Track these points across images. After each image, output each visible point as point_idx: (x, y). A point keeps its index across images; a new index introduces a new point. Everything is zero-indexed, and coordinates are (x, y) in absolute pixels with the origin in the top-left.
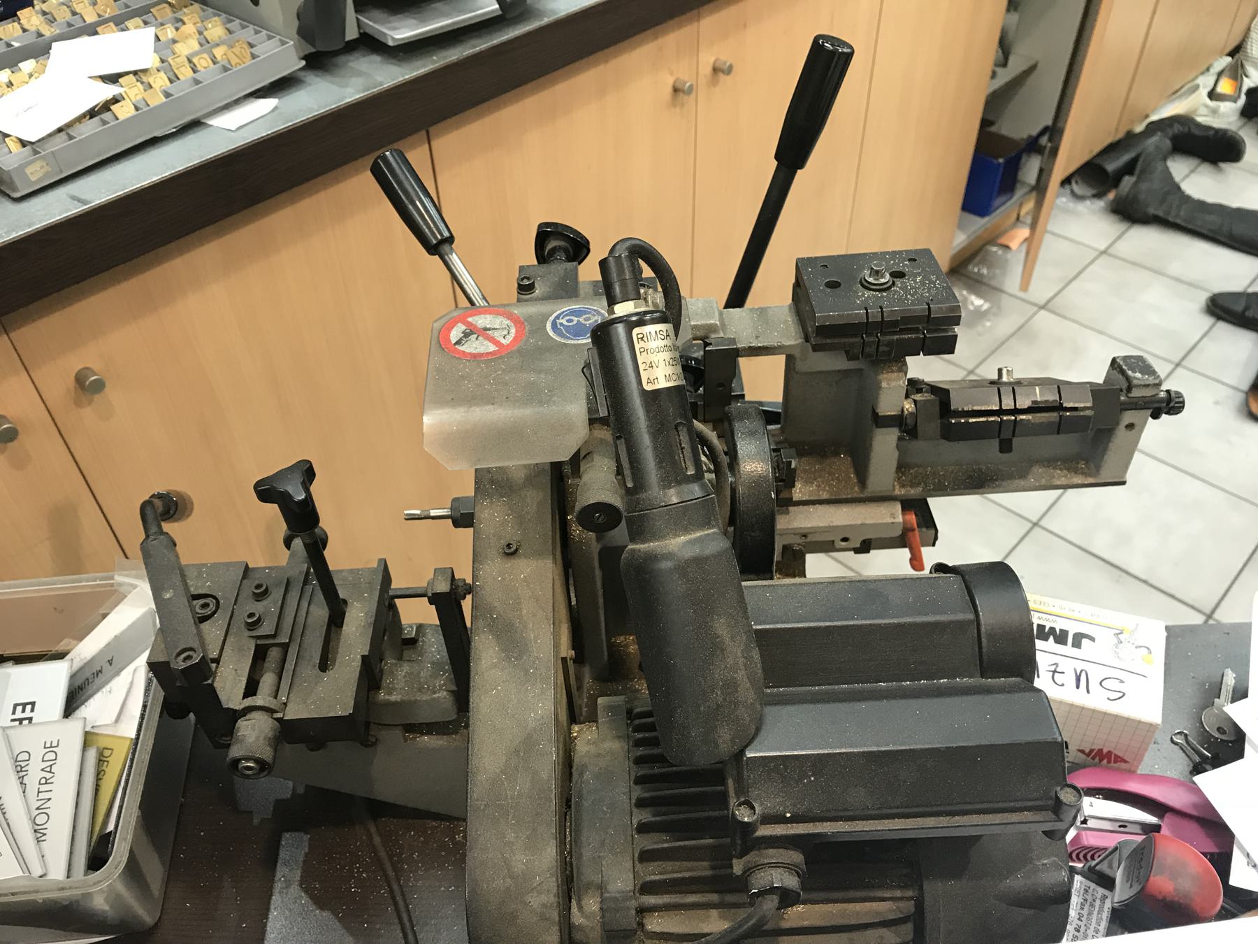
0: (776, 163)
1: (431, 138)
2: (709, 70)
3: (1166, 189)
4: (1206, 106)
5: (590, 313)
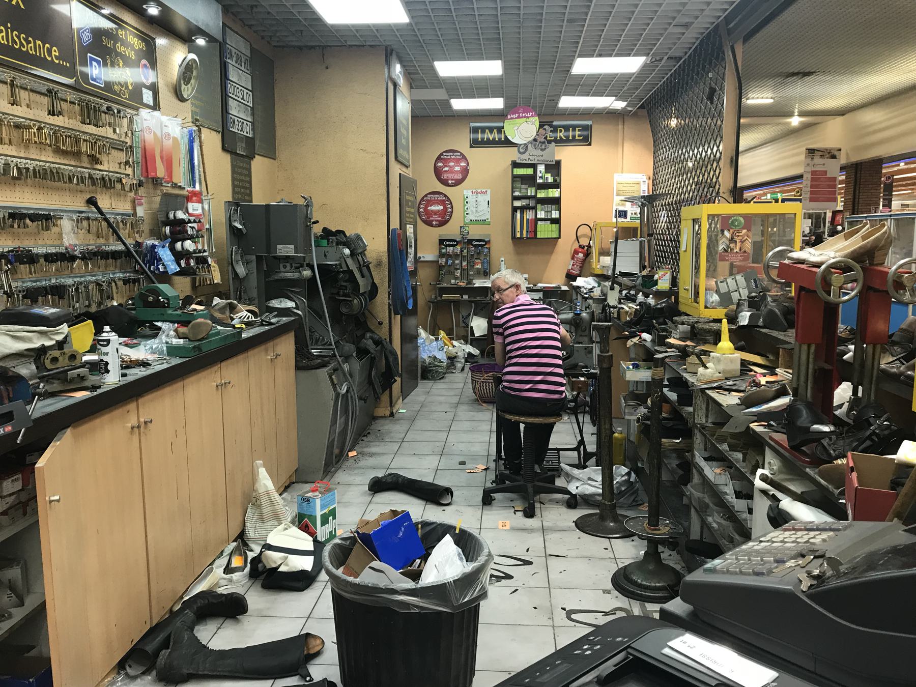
4: (225, 579)
5: (881, 220)
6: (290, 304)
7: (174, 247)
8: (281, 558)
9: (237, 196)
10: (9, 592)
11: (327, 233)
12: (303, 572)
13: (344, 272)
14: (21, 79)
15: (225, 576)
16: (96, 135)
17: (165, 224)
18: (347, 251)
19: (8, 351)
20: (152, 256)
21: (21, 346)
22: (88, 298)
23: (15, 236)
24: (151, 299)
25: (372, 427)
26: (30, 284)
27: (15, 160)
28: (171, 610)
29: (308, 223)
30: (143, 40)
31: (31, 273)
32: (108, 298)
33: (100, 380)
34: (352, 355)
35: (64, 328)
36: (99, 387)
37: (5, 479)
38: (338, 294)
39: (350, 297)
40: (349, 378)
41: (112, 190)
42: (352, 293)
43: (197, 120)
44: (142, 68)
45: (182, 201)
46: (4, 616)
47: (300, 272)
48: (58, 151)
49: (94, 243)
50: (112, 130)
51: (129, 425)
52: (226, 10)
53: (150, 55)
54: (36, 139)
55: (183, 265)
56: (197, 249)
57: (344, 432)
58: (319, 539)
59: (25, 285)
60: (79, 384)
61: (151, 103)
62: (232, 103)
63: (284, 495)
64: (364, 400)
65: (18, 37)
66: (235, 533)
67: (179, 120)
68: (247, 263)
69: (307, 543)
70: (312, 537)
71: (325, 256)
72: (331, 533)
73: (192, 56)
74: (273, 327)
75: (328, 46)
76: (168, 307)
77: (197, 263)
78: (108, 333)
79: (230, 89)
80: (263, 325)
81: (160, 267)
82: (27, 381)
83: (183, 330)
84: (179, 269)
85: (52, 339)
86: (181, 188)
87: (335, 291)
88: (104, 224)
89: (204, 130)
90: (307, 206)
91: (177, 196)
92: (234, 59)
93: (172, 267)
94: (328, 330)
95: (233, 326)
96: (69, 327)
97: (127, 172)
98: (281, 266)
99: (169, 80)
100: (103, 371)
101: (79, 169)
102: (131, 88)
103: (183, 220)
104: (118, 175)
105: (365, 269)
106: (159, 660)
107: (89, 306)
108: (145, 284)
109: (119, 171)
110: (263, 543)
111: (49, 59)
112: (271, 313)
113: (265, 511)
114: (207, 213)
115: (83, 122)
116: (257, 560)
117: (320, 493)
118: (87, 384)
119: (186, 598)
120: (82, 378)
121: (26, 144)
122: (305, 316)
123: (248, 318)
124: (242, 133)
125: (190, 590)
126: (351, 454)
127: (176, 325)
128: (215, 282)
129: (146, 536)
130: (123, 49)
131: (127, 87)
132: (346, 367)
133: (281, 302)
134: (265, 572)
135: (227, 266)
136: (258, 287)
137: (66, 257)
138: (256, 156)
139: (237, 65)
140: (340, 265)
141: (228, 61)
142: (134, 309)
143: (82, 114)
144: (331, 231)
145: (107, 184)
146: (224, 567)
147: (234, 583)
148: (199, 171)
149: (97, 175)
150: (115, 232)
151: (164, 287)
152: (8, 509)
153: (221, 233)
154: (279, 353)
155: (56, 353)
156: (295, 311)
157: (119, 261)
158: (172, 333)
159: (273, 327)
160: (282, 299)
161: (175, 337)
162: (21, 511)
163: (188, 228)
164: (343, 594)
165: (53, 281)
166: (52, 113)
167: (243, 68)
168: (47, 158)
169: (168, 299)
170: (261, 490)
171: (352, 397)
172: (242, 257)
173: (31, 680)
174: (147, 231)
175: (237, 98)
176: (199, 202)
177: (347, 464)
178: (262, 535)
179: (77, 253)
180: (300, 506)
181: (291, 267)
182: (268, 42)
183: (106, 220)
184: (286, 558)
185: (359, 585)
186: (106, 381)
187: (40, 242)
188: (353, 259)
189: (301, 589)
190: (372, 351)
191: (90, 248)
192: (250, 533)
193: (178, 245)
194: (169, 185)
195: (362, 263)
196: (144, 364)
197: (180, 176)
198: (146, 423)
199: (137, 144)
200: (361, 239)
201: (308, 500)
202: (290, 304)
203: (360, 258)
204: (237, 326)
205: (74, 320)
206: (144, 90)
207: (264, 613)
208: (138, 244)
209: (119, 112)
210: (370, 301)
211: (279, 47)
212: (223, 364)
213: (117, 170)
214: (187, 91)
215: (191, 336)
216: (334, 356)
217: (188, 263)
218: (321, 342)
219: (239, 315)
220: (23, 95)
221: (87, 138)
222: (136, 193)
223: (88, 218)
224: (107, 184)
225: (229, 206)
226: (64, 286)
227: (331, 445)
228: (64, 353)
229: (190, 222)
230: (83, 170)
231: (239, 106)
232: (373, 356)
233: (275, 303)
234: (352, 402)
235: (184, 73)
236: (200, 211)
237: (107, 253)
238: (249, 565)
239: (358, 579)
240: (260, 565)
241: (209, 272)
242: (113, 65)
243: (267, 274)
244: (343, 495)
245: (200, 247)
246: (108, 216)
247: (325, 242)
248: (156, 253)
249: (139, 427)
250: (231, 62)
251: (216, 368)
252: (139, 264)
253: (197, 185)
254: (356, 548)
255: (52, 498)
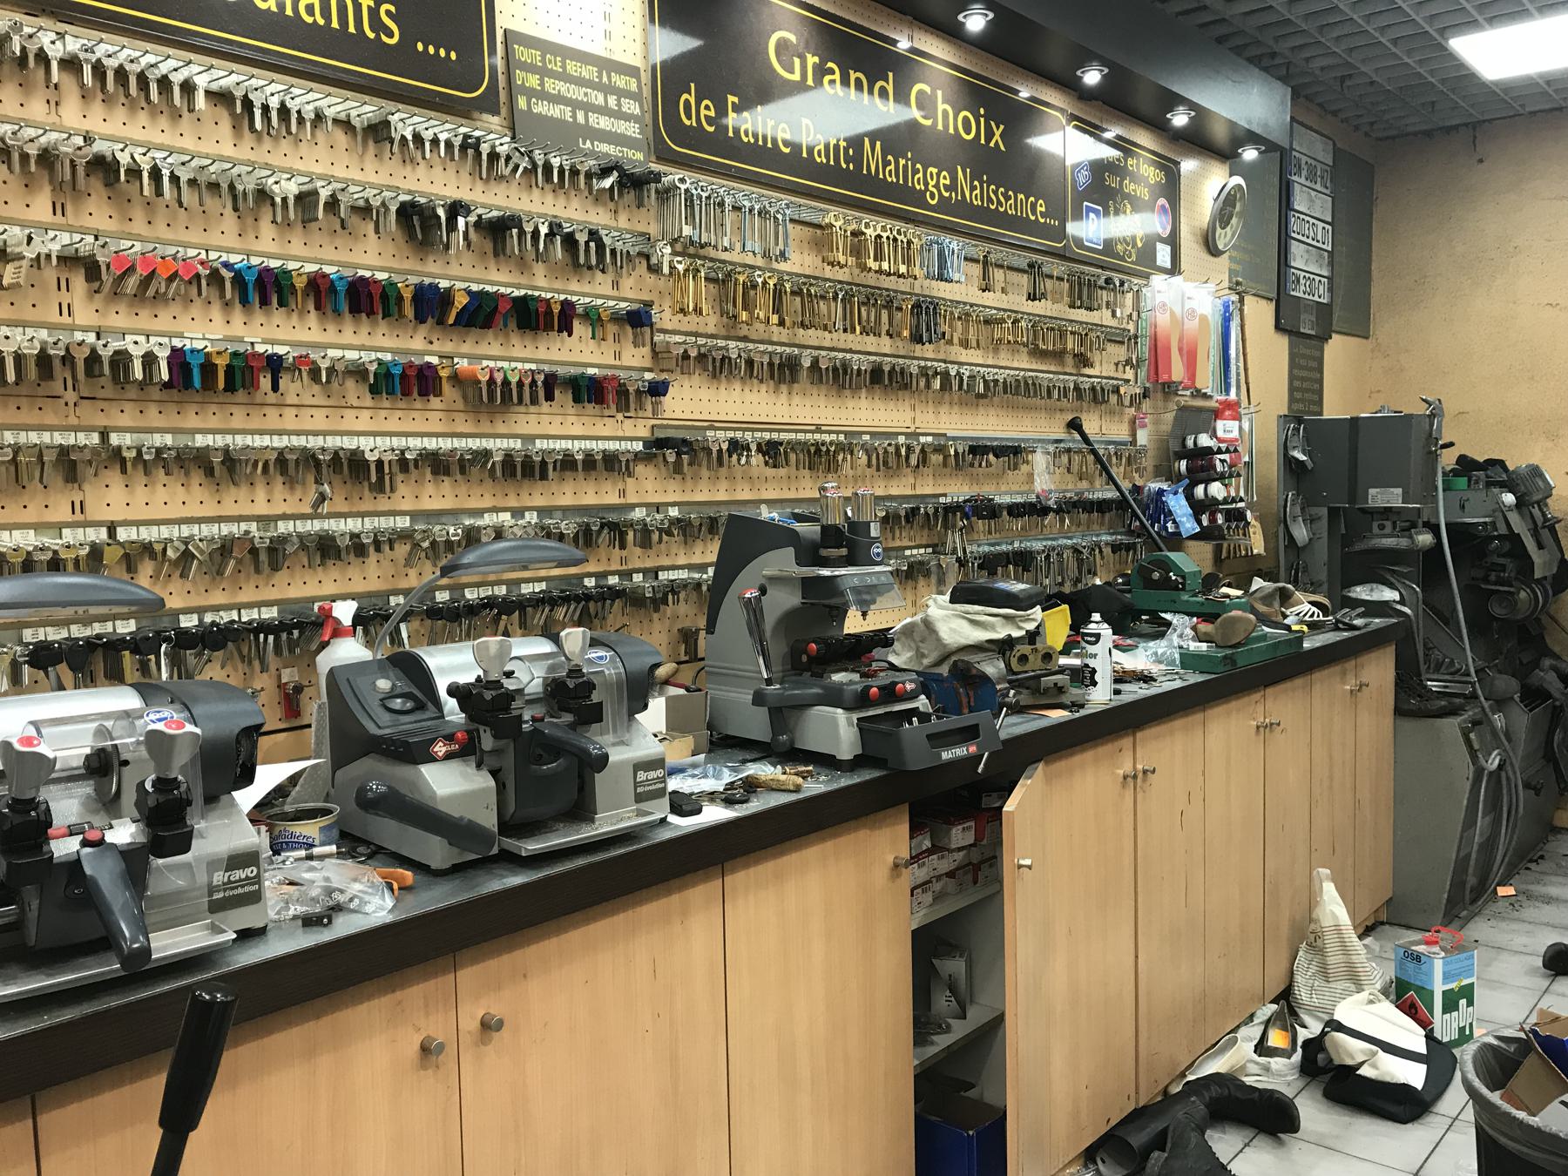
0: (161, 1131)
1: (38, 1112)
2: (476, 1024)
3: (1205, 1168)
4: (1257, 1063)
6: (1389, 595)
7: (1193, 494)
8: (1363, 1052)
9: (1296, 407)
10: (948, 993)
11: (1466, 465)
12: (1406, 1088)
13: (1499, 537)
14: (998, 253)
15: (1255, 1057)
16: (1087, 323)
17: (1180, 457)
18: (1509, 498)
19: (964, 641)
20: (1157, 507)
21: (981, 636)
22: (1061, 572)
23: (975, 479)
24: (1156, 575)
25: (1548, 847)
26: (986, 549)
27: (982, 370)
28: (1165, 1092)
29: (1432, 445)
30: (1162, 167)
31: (990, 533)
32: (1089, 572)
33: (1084, 694)
34: (1512, 698)
35: (1037, 612)
36: (1082, 706)
37: (953, 825)
38: (1486, 580)
39: (1511, 586)
40: (1506, 743)
41: (1104, 406)
42: (1516, 579)
43: (1238, 283)
44: (1159, 213)
45: (1206, 418)
46: (940, 1026)
47: (1411, 537)
48: (1037, 353)
49: (1073, 487)
50: (1109, 313)
51: (1121, 772)
52: (1299, 96)
53: (1171, 188)
54: (1010, 338)
55: (1205, 523)
56: (1229, 496)
57: (1489, 845)
58: (1437, 1034)
59: (981, 549)
60: (1054, 698)
61: (1168, 265)
62: (1296, 248)
63: (1368, 940)
64: (1534, 788)
65: (995, 193)
66: (1276, 989)
67: (1211, 286)
68: (1311, 521)
69: (1414, 1040)
70: (1424, 1028)
71: (1463, 507)
72: (1462, 1030)
73: (1238, 180)
74: (1357, 633)
75: (1484, 121)
76: (1183, 589)
77: (1227, 519)
78: (1097, 625)
79: (1294, 225)
80: (1337, 629)
81: (1169, 525)
82: (994, 685)
83: (1205, 627)
84: (1198, 530)
85: (1021, 628)
86: (1206, 396)
87: (1479, 574)
88: (1091, 458)
89: (1248, 299)
90: (1432, 416)
91: (1200, 410)
92: (1304, 173)
93: (1188, 525)
94: (1464, 649)
95: (1288, 628)
96: (1043, 610)
97: (1126, 376)
98: (1375, 525)
99: (1197, 224)
100: (1087, 682)
101: (1061, 377)
102: (1140, 245)
103: (1210, 448)
104: (1115, 382)
105: (1545, 534)
106: (1149, 1165)
107: (1061, 584)
108: (1143, 555)
109: (1115, 375)
110: (1327, 1018)
111: (1033, 218)
112: (1353, 609)
113: (1331, 960)
114: (1246, 437)
115: (1072, 306)
116: (1314, 1047)
117: (1443, 949)
118: (1066, 699)
119: (1191, 1078)
120: (1060, 690)
121: (996, 345)
122: (1417, 615)
123: (1312, 616)
124: (1311, 297)
125: (1201, 1063)
126: (1502, 891)
127: (1195, 619)
128: (1255, 552)
129: (1137, 957)
130: (1132, 186)
131: (1134, 245)
132: (1498, 720)
133: (1372, 590)
134: (1330, 1070)
135: (1278, 526)
136: (1330, 563)
137: (1035, 510)
138: (1334, 335)
139: (1308, 184)
140: (1493, 523)
141: (1294, 178)
142: (1129, 591)
143: (1071, 294)
144: (1474, 462)
145: (1097, 396)
146: (1255, 1042)
147: (1273, 1074)
148: (1238, 368)
149: (1086, 383)
150: (1105, 469)
151: (1174, 556)
152: (957, 869)
153: (1269, 470)
154: (1364, 680)
155: (1025, 649)
156: (1399, 607)
157: (1107, 515)
158: (1191, 633)
159: (1357, 633)
160: (1374, 586)
161: (1193, 639)
162: (970, 877)
163: (1218, 462)
164: (1503, 1140)
165: (1016, 545)
166: (1032, 297)
167: (1318, 187)
168: (1020, 364)
169: (1183, 577)
170: (1327, 922)
171: (1508, 779)
172: (1303, 509)
173: (971, 1133)
174: (1150, 469)
175: (1304, 239)
176: (1234, 419)
177: (1492, 908)
178: (1326, 1003)
179: (1051, 503)
180: (1400, 966)
181: (1394, 528)
182: (1367, 134)
183: (1094, 452)
184: (1374, 1054)
185: (1538, 1130)
186: (1091, 698)
187: (1003, 488)
188: (1521, 514)
189: (1404, 1121)
190: (1556, 695)
191: (1068, 495)
192: (1302, 993)
193: (1199, 491)
194: (1188, 393)
195: (1540, 523)
196: (1146, 678)
197: (1207, 379)
198: (1145, 772)
199: (1145, 329)
200: (1541, 476)
201: (1417, 958)
202: (1389, 595)
203: (1536, 511)
204: (1294, 628)
205: (1048, 602)
206: (1159, 246)
207: (1329, 1143)
208: (1137, 490)
209: (1122, 284)
210: (1554, 595)
211: (1387, 138)
212: (1270, 691)
213: (1112, 374)
214: (1224, 238)
215: (1218, 639)
216: (1474, 696)
217: (1213, 520)
218: (1447, 668)
219: (1296, 609)
220: (998, 275)
221: (1076, 328)
222: (1138, 409)
223: (1069, 450)
224: (1097, 396)
225: (1285, 423)
226: (1031, 553)
227: (1461, 865)
228: (1036, 650)
229: (1220, 451)
230: (1067, 377)
231: (1308, 251)
232: (1558, 703)
233: (1361, 592)
234: (1509, 790)
235: (1221, 210)
236: (1235, 434)
237: (1092, 503)
238: (1299, 1050)
239: (1536, 1119)
240: (1320, 1056)
241: (1244, 535)
242: (1117, 213)
243: (1347, 541)
244: (1488, 965)
245: (1233, 494)
246: (1096, 446)
247: (1462, 482)
248: (1163, 502)
249: (1135, 777)
250: (1298, 180)
251: (1257, 696)
252: (1138, 518)
253: (1233, 391)
254: (1531, 1062)
255: (1022, 862)
